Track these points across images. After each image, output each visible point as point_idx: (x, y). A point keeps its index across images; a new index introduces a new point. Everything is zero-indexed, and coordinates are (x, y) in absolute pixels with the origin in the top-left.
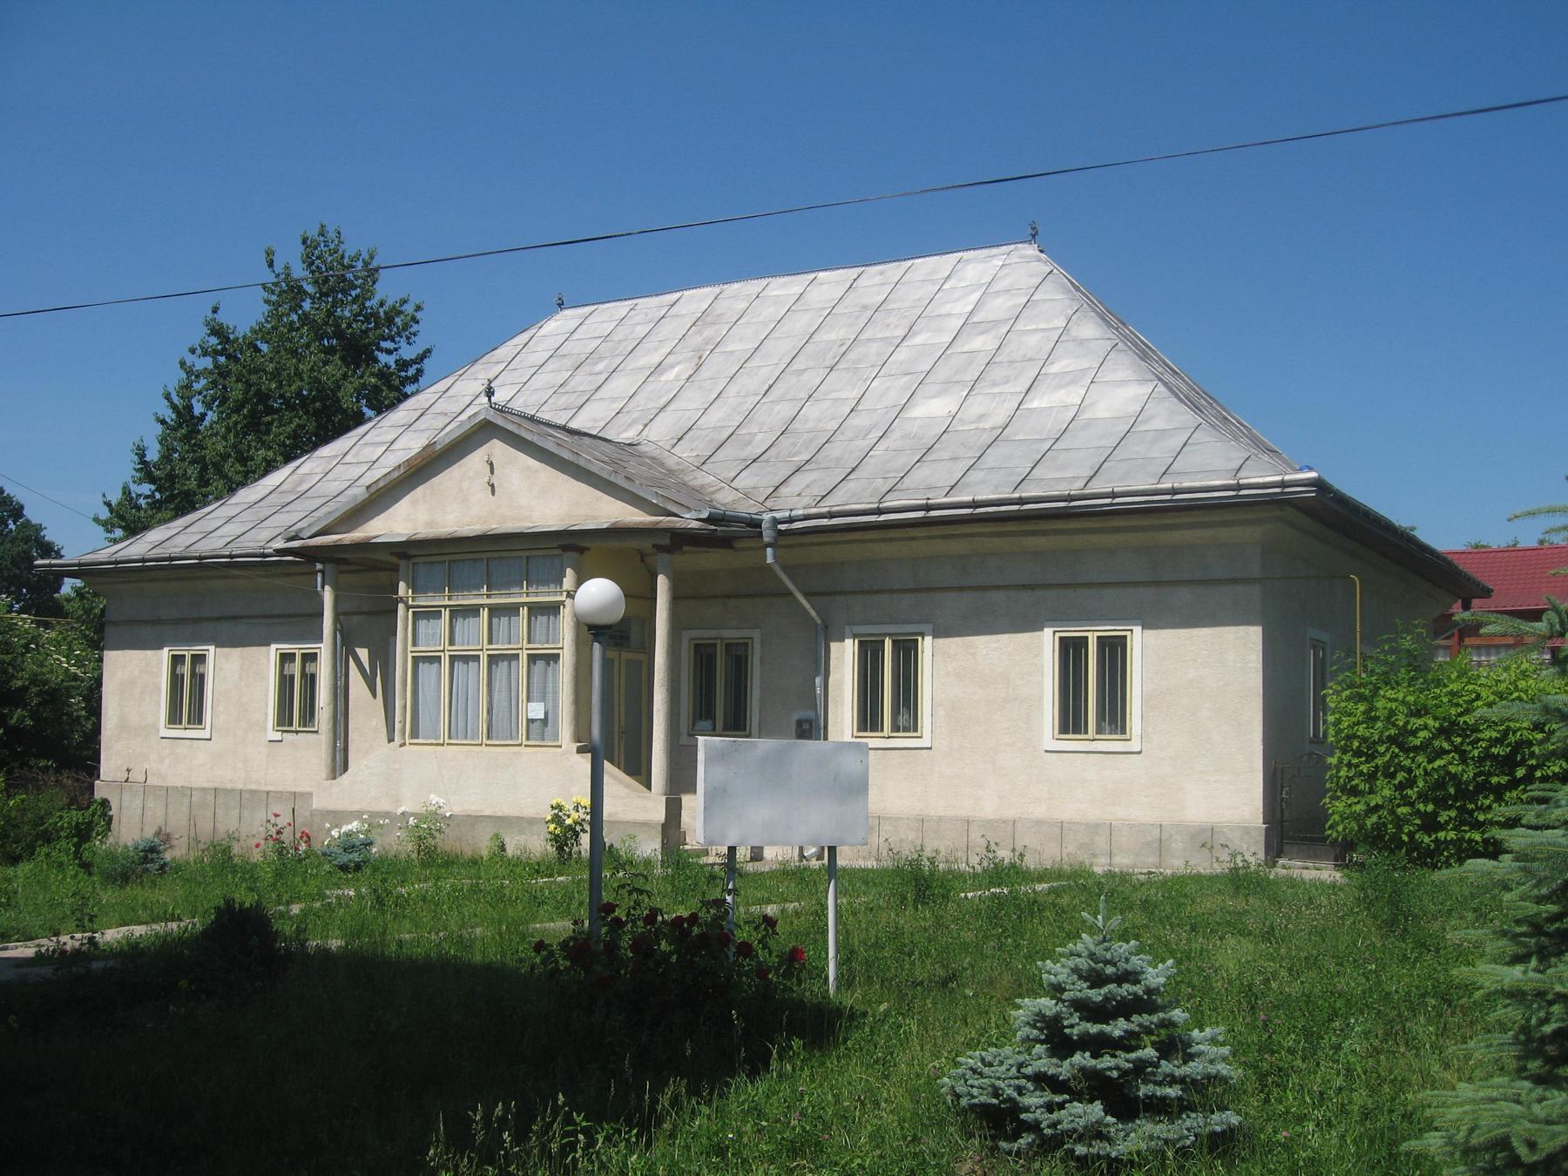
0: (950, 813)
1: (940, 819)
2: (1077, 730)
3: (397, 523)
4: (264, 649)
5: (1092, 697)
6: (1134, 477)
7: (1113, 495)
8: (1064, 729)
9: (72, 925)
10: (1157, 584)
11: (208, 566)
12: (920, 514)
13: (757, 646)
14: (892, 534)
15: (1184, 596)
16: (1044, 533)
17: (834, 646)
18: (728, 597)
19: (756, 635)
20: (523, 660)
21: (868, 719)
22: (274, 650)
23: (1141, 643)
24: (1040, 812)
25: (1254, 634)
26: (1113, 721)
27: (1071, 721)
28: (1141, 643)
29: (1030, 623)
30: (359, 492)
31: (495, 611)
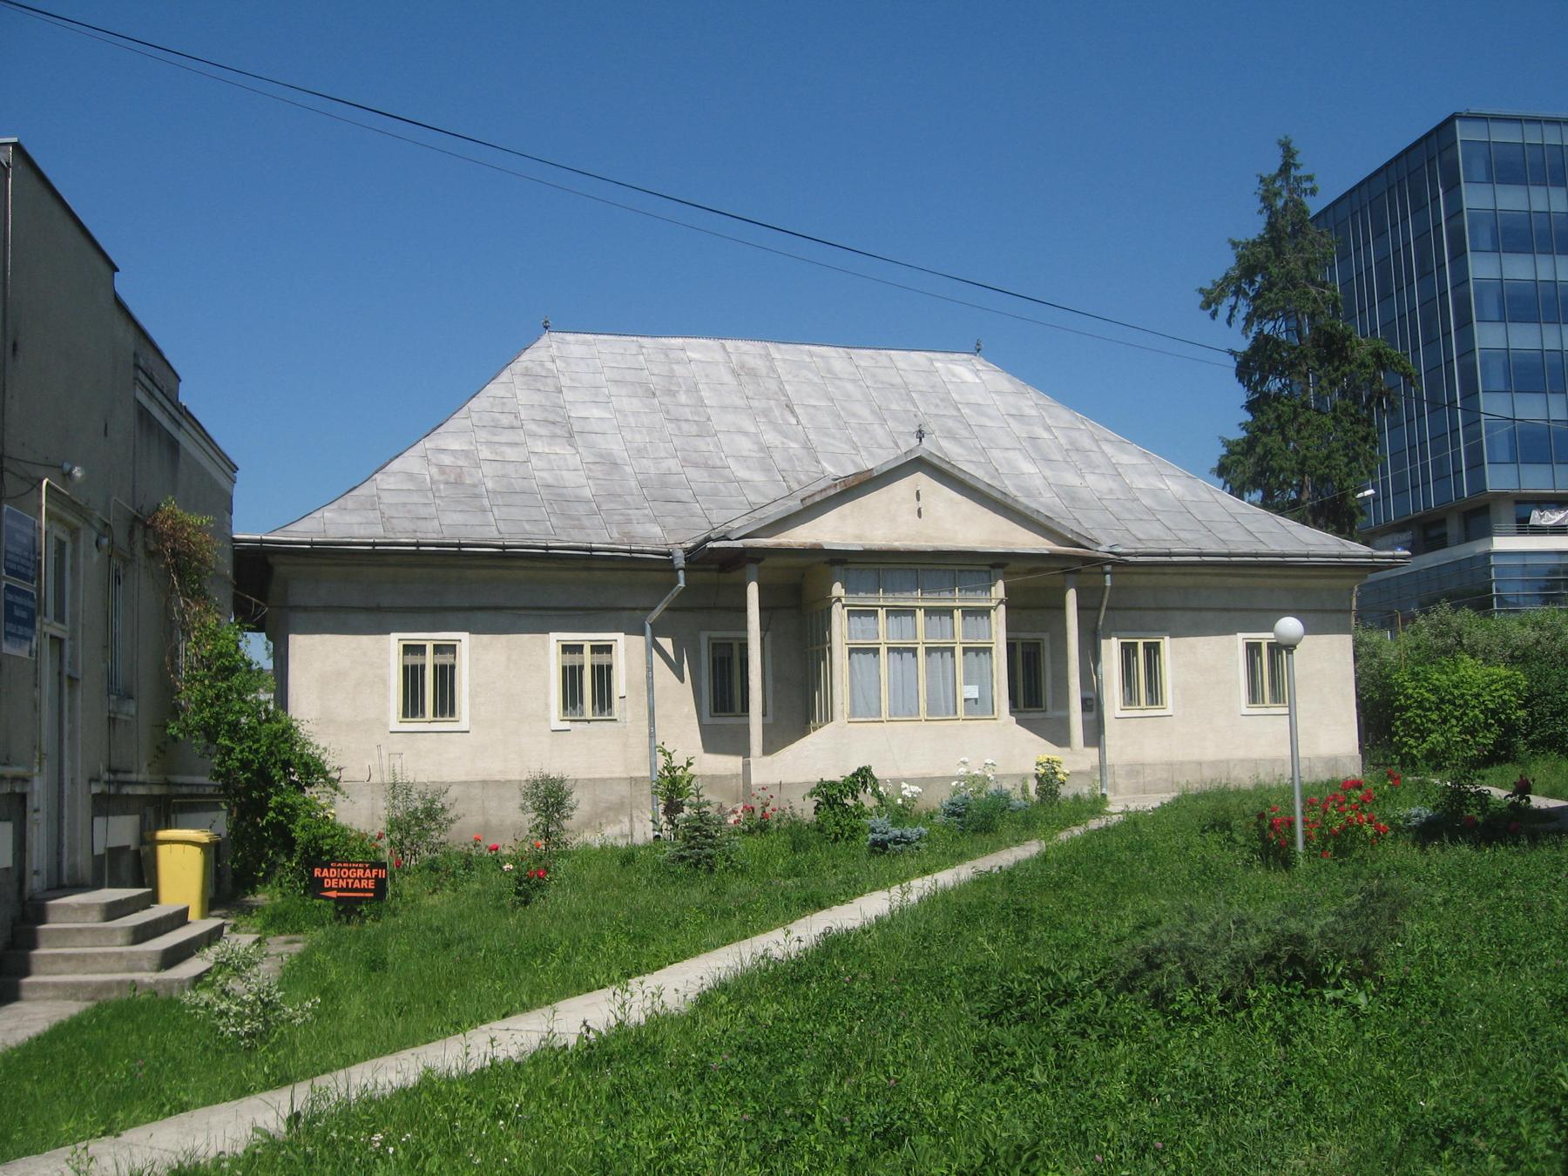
1: (1182, 763)
3: (832, 531)
4: (1225, 639)
5: (1269, 676)
6: (1187, 539)
8: (405, 715)
13: (1047, 644)
14: (1183, 570)
16: (1244, 576)
17: (1103, 642)
19: (1046, 637)
21: (1130, 697)
22: (555, 639)
23: (1166, 644)
24: (1241, 754)
25: (292, 637)
27: (1254, 696)
28: (1166, 644)
29: (1228, 630)
31: (968, 612)
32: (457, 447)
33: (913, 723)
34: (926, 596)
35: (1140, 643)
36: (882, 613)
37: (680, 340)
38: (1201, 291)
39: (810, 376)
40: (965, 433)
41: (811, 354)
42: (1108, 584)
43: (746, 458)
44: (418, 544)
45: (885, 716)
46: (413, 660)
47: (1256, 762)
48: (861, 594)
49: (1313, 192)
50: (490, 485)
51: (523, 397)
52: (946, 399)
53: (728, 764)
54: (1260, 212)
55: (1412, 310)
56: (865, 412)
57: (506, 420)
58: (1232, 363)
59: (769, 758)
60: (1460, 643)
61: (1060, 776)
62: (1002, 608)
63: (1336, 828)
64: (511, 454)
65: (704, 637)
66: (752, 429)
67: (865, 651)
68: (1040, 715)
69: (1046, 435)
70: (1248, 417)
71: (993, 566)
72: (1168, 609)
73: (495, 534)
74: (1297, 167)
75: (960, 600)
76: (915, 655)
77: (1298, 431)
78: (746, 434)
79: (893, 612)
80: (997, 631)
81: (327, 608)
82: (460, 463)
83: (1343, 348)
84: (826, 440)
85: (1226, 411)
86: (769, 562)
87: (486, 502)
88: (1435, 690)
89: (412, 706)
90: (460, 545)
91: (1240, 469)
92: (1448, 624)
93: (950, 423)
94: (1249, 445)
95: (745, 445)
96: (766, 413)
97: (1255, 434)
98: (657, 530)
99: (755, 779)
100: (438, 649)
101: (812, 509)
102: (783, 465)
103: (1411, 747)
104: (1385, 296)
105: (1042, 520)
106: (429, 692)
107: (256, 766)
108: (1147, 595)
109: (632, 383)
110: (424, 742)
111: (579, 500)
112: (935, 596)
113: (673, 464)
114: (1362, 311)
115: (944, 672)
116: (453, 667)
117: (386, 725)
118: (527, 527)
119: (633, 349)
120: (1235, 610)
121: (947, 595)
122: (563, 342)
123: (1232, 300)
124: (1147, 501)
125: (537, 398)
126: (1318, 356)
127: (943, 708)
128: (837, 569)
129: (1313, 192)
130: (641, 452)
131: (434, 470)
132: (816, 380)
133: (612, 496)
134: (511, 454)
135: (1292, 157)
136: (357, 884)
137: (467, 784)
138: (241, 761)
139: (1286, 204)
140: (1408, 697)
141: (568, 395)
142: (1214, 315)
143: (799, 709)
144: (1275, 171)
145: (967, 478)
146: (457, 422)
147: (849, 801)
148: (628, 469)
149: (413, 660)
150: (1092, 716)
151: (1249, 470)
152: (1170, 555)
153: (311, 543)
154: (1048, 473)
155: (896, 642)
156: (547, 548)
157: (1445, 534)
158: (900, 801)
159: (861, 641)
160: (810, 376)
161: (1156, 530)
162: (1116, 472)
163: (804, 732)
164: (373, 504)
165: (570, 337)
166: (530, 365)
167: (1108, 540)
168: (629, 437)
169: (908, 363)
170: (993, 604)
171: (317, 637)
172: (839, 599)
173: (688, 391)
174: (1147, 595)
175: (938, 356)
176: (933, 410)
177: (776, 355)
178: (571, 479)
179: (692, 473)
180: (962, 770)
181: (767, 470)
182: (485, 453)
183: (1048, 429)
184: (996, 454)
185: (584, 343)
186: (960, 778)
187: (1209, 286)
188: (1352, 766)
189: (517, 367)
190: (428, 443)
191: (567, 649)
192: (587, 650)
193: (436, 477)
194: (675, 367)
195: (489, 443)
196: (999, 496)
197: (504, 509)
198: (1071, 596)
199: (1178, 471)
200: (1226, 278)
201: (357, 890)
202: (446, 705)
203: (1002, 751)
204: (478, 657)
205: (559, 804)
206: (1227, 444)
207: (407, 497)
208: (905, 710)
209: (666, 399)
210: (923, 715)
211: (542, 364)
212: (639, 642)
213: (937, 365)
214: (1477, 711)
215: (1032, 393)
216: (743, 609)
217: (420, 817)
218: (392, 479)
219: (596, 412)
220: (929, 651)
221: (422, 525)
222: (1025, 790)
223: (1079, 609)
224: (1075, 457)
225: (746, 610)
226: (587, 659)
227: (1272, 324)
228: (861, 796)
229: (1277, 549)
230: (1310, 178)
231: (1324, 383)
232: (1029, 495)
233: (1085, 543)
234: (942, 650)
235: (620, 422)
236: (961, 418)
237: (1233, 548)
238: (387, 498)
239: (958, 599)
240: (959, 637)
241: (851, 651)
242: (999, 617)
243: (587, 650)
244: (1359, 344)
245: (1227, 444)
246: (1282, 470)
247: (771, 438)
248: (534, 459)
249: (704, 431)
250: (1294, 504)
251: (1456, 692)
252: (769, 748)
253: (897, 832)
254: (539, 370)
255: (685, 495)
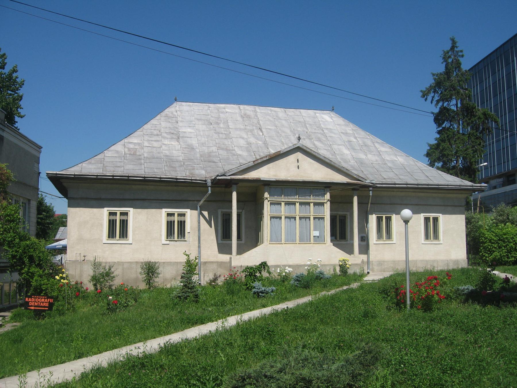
0: (401, 259)
1: (399, 261)
2: (113, 237)
3: (264, 173)
4: (419, 215)
5: (432, 230)
7: (448, 185)
8: (109, 237)
9: (58, 316)
10: (444, 206)
11: (377, 187)
12: (405, 186)
14: (389, 190)
15: (450, 208)
17: (370, 216)
18: (340, 203)
20: (297, 218)
22: (164, 211)
24: (421, 258)
26: (181, 234)
27: (427, 237)
28: (442, 218)
30: (252, 164)
31: (315, 204)
32: (136, 142)
33: (293, 246)
34: (300, 198)
35: (384, 216)
36: (283, 204)
37: (224, 105)
38: (421, 91)
39: (270, 118)
40: (324, 139)
41: (271, 111)
42: (371, 194)
43: (241, 147)
44: (113, 176)
45: (283, 242)
46: (112, 218)
47: (427, 261)
48: (276, 197)
49: (462, 56)
50: (146, 155)
51: (164, 124)
52: (319, 127)
53: (225, 258)
54: (442, 63)
55: (504, 100)
56: (288, 131)
57: (155, 132)
58: (432, 118)
59: (238, 256)
60: (508, 218)
61: (347, 266)
62: (329, 203)
63: (424, 296)
64: (155, 144)
65: (220, 212)
66: (246, 137)
67: (276, 218)
68: (345, 242)
69: (354, 140)
70: (438, 136)
71: (325, 187)
72: (394, 204)
73: (143, 173)
74: (457, 47)
75: (313, 199)
76: (295, 220)
77: (455, 141)
78: (243, 138)
79: (287, 204)
80: (327, 211)
81: (82, 199)
82: (136, 147)
83: (473, 112)
84: (272, 141)
85: (430, 134)
86: (240, 184)
87: (143, 161)
88: (496, 236)
89: (111, 234)
90: (128, 177)
91: (434, 154)
92: (504, 212)
93: (319, 135)
94: (438, 145)
95: (242, 142)
96: (251, 131)
97: (441, 141)
98: (203, 172)
99: (233, 264)
100: (122, 214)
101: (257, 165)
102: (255, 149)
103: (486, 257)
104: (495, 95)
105: (345, 170)
106: (118, 229)
107: (18, 257)
108: (381, 199)
109: (204, 120)
110: (115, 247)
111: (177, 161)
112: (303, 198)
113: (214, 149)
114: (487, 101)
115: (306, 225)
116: (127, 221)
117: (102, 241)
118: (156, 170)
119: (206, 108)
120: (420, 205)
121: (308, 197)
122: (181, 105)
123: (432, 94)
124: (390, 165)
125: (169, 125)
126: (463, 114)
127: (305, 239)
128: (266, 187)
129: (462, 56)
130: (203, 144)
131: (126, 150)
132: (272, 119)
133: (190, 160)
134: (155, 144)
135: (455, 43)
136: (42, 304)
137: (130, 263)
138: (12, 255)
139: (453, 60)
140: (486, 238)
141: (180, 124)
142: (426, 100)
143: (251, 237)
144: (449, 49)
145: (316, 155)
146: (138, 133)
147: (258, 274)
148: (198, 150)
149: (112, 218)
150: (364, 243)
151: (437, 156)
152: (395, 184)
153: (75, 175)
154: (353, 154)
155: (288, 214)
156: (160, 178)
157: (515, 179)
158: (284, 274)
159: (275, 214)
160: (270, 118)
161: (391, 175)
162: (379, 154)
163: (256, 246)
164: (101, 161)
165: (184, 104)
166: (167, 113)
167: (371, 177)
168: (200, 139)
169: (306, 114)
170: (325, 201)
171: (78, 209)
172: (267, 199)
173: (224, 123)
174: (381, 199)
175: (318, 111)
176: (314, 131)
177: (258, 111)
178: (175, 153)
179: (221, 152)
180: (309, 263)
181: (248, 151)
182: (146, 144)
183: (356, 138)
184: (335, 147)
185: (189, 106)
186: (309, 265)
187: (424, 90)
188: (464, 264)
189: (163, 114)
190: (126, 140)
191: (169, 215)
192: (176, 215)
193: (127, 152)
194: (221, 114)
195: (148, 140)
196: (328, 161)
197: (149, 164)
198: (355, 199)
199: (403, 154)
200: (431, 86)
201: (42, 307)
202: (124, 234)
203: (326, 256)
204: (136, 217)
205: (153, 273)
206: (430, 145)
207: (116, 159)
208: (290, 240)
209: (215, 126)
210: (298, 242)
211: (172, 113)
212: (195, 213)
213: (317, 115)
214: (512, 244)
215: (351, 125)
216: (231, 201)
217: (103, 276)
218: (110, 153)
219: (189, 130)
220: (300, 218)
221: (117, 169)
222: (335, 270)
223: (358, 203)
224: (364, 148)
225: (235, 201)
226: (176, 219)
227: (447, 103)
228: (263, 273)
229: (436, 182)
230: (461, 51)
231: (465, 124)
232: (345, 161)
233: (361, 179)
234: (306, 218)
235: (197, 134)
236: (324, 134)
237: (449, 183)
238: (107, 159)
239: (312, 199)
240: (312, 214)
241: (271, 218)
242: (327, 206)
243: (176, 215)
244: (479, 110)
245: (430, 145)
246: (448, 155)
247: (252, 140)
248: (163, 147)
249: (228, 137)
250: (454, 167)
251: (504, 236)
252: (240, 251)
253: (263, 289)
254: (171, 115)
255: (215, 159)
